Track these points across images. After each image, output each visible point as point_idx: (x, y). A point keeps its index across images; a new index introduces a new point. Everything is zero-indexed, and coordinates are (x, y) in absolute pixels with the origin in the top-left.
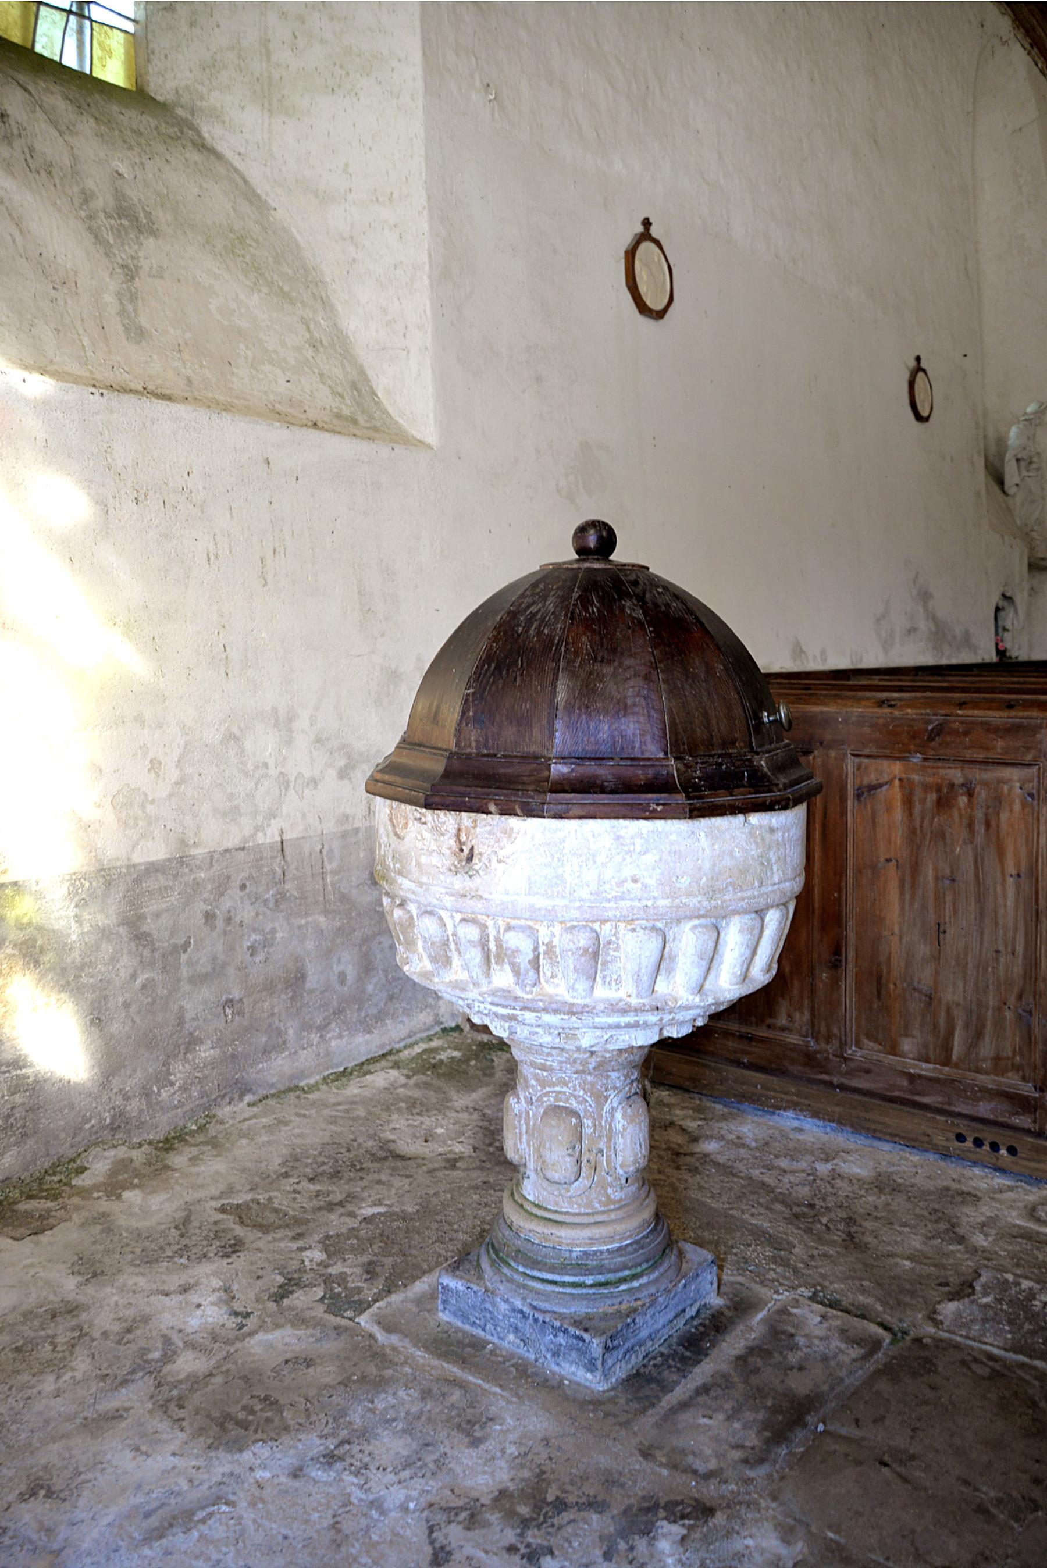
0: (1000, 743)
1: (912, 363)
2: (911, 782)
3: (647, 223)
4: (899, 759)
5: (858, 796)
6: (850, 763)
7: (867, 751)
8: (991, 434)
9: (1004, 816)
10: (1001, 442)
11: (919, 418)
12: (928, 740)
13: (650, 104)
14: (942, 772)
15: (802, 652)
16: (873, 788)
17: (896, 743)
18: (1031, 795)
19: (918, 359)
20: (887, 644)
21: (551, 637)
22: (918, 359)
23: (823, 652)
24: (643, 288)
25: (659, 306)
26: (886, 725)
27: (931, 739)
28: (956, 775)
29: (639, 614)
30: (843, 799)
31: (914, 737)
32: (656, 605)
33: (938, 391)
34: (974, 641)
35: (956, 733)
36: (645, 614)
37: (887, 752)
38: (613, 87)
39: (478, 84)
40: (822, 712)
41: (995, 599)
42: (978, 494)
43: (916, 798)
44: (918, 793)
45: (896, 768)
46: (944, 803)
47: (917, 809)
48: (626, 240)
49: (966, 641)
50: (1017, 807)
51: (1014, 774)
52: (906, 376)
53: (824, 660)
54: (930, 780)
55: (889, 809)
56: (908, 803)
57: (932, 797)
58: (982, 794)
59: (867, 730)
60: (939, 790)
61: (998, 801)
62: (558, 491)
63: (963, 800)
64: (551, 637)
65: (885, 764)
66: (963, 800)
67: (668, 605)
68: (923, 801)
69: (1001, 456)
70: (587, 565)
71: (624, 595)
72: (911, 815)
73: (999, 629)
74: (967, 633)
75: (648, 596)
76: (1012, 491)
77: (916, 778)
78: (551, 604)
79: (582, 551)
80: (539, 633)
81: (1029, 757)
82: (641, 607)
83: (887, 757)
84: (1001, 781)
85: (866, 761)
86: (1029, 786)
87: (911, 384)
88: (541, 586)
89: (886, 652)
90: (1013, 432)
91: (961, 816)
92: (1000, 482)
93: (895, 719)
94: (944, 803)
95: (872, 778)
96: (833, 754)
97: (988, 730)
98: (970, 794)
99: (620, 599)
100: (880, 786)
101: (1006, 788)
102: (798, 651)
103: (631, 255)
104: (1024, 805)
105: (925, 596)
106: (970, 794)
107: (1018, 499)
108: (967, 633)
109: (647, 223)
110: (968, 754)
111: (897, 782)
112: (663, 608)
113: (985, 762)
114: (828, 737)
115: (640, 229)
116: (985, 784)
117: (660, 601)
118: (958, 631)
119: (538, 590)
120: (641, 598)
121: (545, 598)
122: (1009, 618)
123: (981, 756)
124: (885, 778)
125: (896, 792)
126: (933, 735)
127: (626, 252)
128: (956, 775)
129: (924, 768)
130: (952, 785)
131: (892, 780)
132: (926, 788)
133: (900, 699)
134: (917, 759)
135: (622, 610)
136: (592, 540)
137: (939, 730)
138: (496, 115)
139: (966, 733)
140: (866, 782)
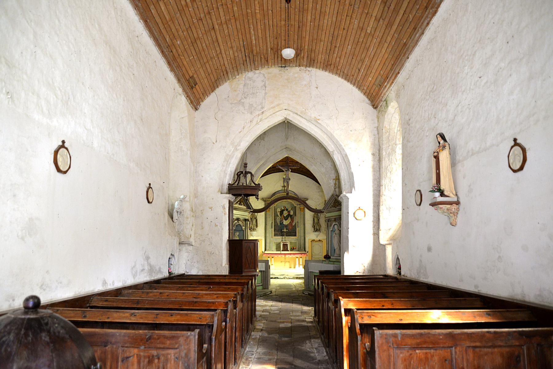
0: (168, 342)
1: (148, 185)
2: (140, 355)
3: (63, 142)
4: (137, 348)
5: (123, 361)
6: (120, 350)
7: (126, 345)
8: (170, 203)
9: (169, 365)
10: (173, 205)
11: (149, 202)
12: (147, 341)
13: (69, 103)
14: (150, 351)
15: (106, 283)
16: (127, 358)
17: (136, 342)
18: (177, 358)
19: (150, 184)
20: (134, 276)
21: (11, 352)
22: (150, 184)
23: (113, 282)
24: (60, 164)
25: (65, 170)
26: (133, 336)
27: (147, 341)
28: (154, 352)
29: (47, 339)
30: (117, 362)
31: (142, 340)
32: (54, 333)
33: (155, 195)
34: (162, 270)
35: (155, 339)
36: (50, 338)
37: (133, 345)
38: (56, 97)
39: (4, 91)
40: (112, 332)
41: (169, 256)
42: (165, 224)
43: (142, 361)
44: (142, 359)
45: (136, 351)
46: (150, 362)
47: (142, 364)
48: (55, 147)
49: (160, 271)
50: (173, 362)
51: (172, 352)
52: (146, 189)
53: (113, 285)
54: (146, 354)
55: (133, 365)
56: (139, 362)
57: (147, 360)
58: (162, 358)
59: (127, 338)
60: (149, 358)
61: (167, 360)
62: (18, 236)
63: (156, 361)
64: (11, 352)
65: (132, 349)
66: (156, 361)
67: (59, 332)
68: (144, 362)
69: (173, 210)
70: (28, 316)
71: (42, 330)
72: (140, 366)
73: (170, 264)
74: (160, 268)
75: (52, 329)
76: (175, 221)
77: (142, 354)
78: (12, 337)
79: (26, 307)
80: (6, 350)
81: (176, 346)
82: (49, 336)
83: (133, 347)
84: (168, 354)
85: (126, 349)
86: (176, 355)
87: (147, 192)
88: (8, 327)
89: (134, 278)
90: (176, 203)
91: (156, 366)
92: (172, 218)
93: (136, 334)
94: (150, 362)
95: (128, 354)
96: (115, 346)
97: (165, 338)
98: (159, 358)
99: (41, 332)
100: (130, 357)
101: (169, 356)
102: (105, 283)
103: (56, 152)
104: (175, 361)
105: (148, 258)
106: (159, 358)
107: (177, 224)
108: (160, 268)
109: (63, 142)
110: (158, 346)
111: (136, 356)
112: (57, 334)
113: (164, 348)
114: (113, 340)
115: (61, 144)
116: (163, 355)
117: (56, 331)
118: (157, 268)
119: (7, 330)
120: (49, 331)
121: (9, 333)
122: (172, 261)
123: (162, 346)
124: (132, 354)
125: (135, 359)
126: (148, 340)
127: (55, 151)
128: (154, 352)
129: (144, 351)
130: (153, 356)
131: (134, 355)
132: (145, 357)
133: (138, 313)
134: (142, 347)
135: (41, 338)
136: (31, 304)
137: (150, 338)
138: (10, 103)
139: (158, 339)
140: (125, 356)
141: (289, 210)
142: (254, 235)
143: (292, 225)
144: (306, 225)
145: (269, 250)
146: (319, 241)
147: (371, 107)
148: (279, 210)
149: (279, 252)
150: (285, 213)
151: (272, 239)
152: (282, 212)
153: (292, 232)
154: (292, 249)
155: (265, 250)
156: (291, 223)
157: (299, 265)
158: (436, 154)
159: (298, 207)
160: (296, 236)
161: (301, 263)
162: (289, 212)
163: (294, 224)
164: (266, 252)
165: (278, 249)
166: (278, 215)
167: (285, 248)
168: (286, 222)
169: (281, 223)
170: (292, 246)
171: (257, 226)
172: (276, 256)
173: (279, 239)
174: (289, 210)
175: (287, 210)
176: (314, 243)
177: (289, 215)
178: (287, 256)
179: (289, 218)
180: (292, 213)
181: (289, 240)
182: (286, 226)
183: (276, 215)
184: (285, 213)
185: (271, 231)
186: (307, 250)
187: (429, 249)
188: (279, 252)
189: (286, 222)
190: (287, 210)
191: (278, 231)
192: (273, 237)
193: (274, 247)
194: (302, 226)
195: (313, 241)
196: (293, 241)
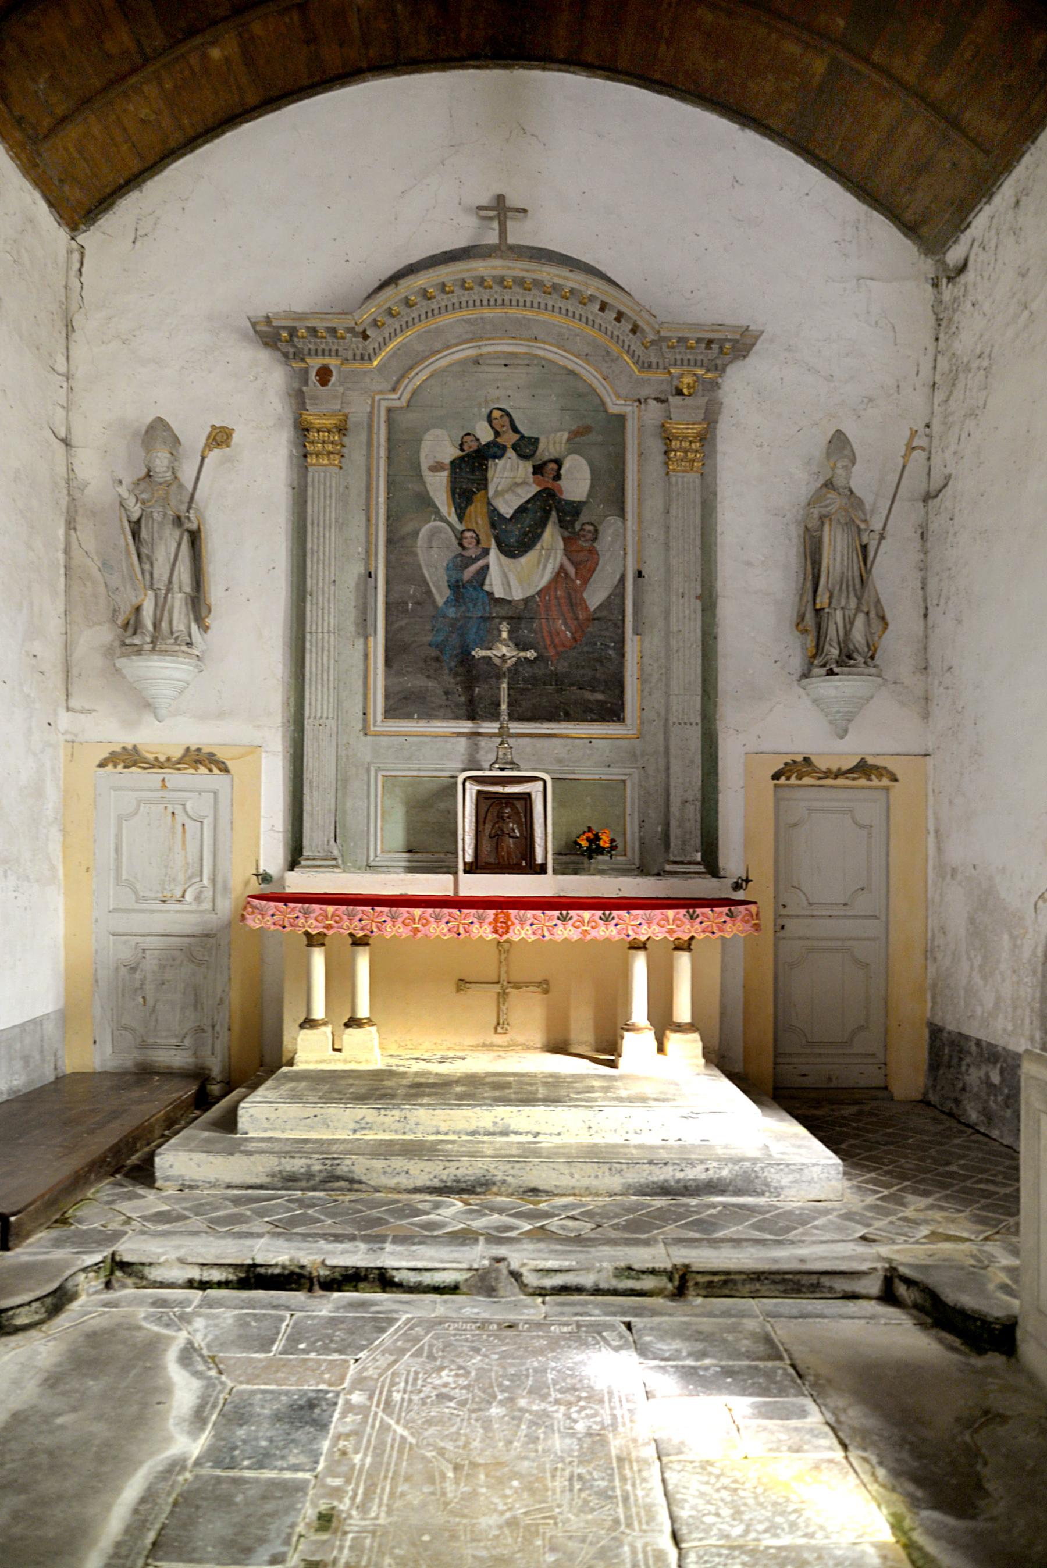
141: (548, 449)
142: (163, 693)
143: (574, 601)
144: (727, 610)
145: (330, 862)
146: (863, 769)
147: (752, 360)
148: (440, 448)
149: (436, 885)
150: (510, 484)
151: (363, 748)
152: (471, 467)
153: (580, 684)
154: (581, 852)
155: (295, 859)
156: (567, 586)
157: (663, 1023)
158: (921, 565)
159: (641, 422)
160: (613, 712)
161: (683, 1012)
162: (547, 470)
163: (595, 597)
164: (298, 882)
165: (429, 848)
166: (425, 502)
167: (506, 841)
168: (511, 578)
169: (467, 587)
170: (585, 816)
171: (198, 604)
172: (394, 927)
173: (441, 748)
174: (548, 449)
175: (526, 447)
176: (805, 796)
177: (547, 505)
178: (524, 929)
179: (551, 536)
180: (576, 482)
181: (552, 761)
182: (519, 616)
183: (406, 505)
184: (510, 484)
185: (354, 664)
186: (732, 860)
187: (974, 867)
188: (436, 885)
189: (511, 578)
190: (526, 447)
191: (432, 664)
192: (379, 722)
193: (389, 830)
194: (686, 618)
195: (795, 770)
196: (588, 771)
